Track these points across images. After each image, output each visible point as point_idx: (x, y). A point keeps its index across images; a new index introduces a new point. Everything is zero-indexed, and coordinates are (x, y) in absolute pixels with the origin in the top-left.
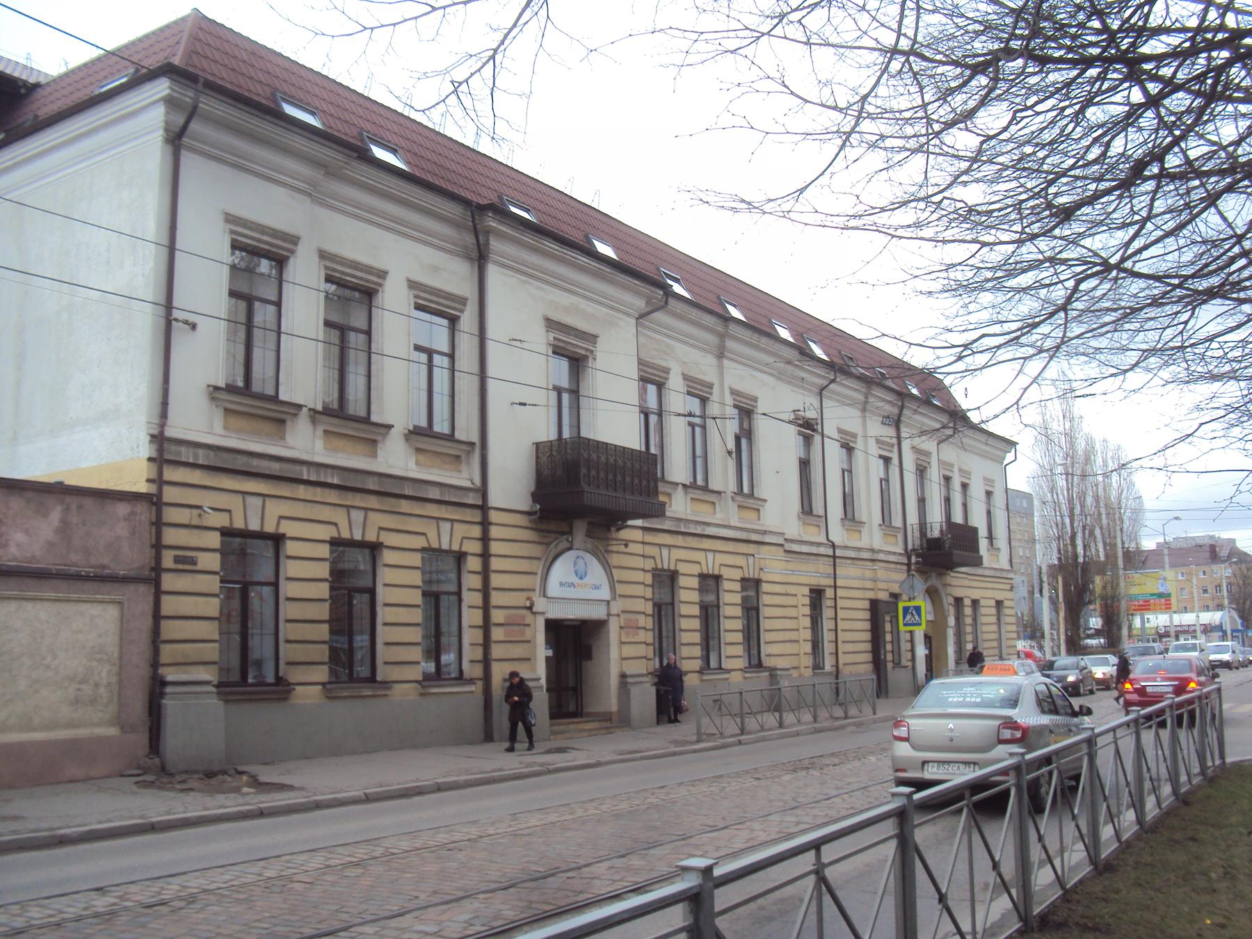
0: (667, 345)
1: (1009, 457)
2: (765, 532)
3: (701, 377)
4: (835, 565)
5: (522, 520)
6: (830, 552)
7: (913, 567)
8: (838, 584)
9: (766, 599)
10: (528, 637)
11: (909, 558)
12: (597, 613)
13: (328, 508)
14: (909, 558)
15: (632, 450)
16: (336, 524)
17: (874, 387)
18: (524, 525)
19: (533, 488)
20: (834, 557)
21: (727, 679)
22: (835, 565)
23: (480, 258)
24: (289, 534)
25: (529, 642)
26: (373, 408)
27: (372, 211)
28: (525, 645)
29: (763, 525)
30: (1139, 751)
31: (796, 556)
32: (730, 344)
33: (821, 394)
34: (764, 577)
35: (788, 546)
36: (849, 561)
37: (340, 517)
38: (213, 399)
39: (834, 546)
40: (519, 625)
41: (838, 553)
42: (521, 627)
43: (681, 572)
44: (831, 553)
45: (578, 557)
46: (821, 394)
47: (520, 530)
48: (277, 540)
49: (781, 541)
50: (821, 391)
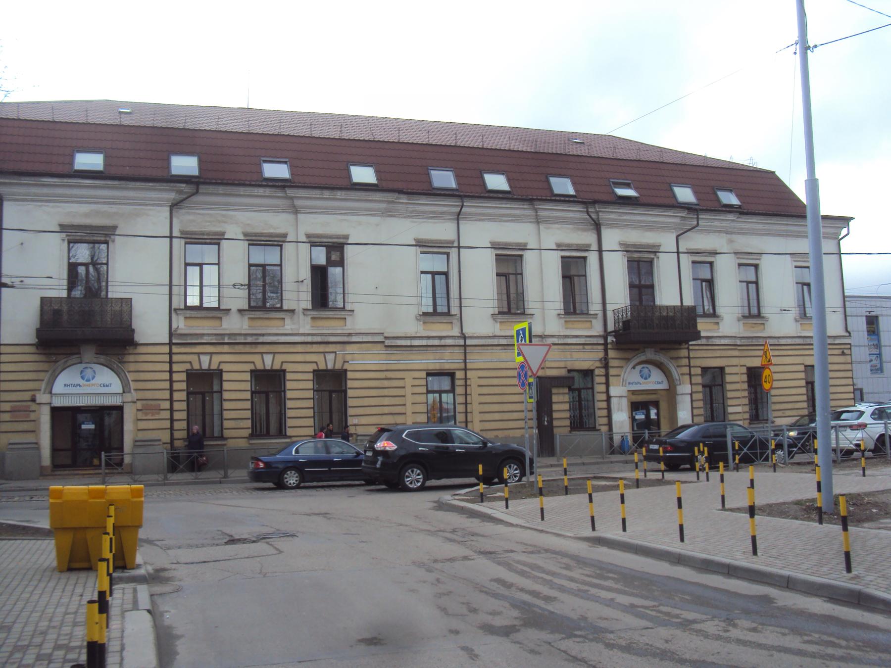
0: (223, 216)
1: (844, 232)
2: (350, 335)
3: (272, 231)
4: (465, 353)
5: (32, 349)
6: (461, 342)
7: (609, 346)
8: (468, 367)
9: (226, 386)
10: (33, 416)
11: (605, 338)
12: (116, 401)
13: (300, 355)
14: (605, 338)
15: (674, 307)
16: (253, 362)
17: (535, 203)
18: (32, 352)
19: (38, 326)
20: (465, 346)
21: (225, 445)
22: (465, 353)
23: (597, 227)
24: (348, 369)
25: (34, 421)
26: (221, 304)
27: (71, 196)
28: (33, 423)
29: (224, 329)
30: (49, 613)
31: (404, 349)
32: (298, 203)
33: (458, 220)
34: (346, 366)
35: (388, 342)
36: (500, 348)
37: (319, 358)
38: (494, 319)
39: (464, 337)
40: (27, 411)
41: (469, 342)
42: (28, 413)
43: (224, 370)
44: (463, 343)
45: (643, 368)
46: (458, 220)
47: (31, 355)
48: (220, 372)
49: (380, 338)
50: (458, 217)
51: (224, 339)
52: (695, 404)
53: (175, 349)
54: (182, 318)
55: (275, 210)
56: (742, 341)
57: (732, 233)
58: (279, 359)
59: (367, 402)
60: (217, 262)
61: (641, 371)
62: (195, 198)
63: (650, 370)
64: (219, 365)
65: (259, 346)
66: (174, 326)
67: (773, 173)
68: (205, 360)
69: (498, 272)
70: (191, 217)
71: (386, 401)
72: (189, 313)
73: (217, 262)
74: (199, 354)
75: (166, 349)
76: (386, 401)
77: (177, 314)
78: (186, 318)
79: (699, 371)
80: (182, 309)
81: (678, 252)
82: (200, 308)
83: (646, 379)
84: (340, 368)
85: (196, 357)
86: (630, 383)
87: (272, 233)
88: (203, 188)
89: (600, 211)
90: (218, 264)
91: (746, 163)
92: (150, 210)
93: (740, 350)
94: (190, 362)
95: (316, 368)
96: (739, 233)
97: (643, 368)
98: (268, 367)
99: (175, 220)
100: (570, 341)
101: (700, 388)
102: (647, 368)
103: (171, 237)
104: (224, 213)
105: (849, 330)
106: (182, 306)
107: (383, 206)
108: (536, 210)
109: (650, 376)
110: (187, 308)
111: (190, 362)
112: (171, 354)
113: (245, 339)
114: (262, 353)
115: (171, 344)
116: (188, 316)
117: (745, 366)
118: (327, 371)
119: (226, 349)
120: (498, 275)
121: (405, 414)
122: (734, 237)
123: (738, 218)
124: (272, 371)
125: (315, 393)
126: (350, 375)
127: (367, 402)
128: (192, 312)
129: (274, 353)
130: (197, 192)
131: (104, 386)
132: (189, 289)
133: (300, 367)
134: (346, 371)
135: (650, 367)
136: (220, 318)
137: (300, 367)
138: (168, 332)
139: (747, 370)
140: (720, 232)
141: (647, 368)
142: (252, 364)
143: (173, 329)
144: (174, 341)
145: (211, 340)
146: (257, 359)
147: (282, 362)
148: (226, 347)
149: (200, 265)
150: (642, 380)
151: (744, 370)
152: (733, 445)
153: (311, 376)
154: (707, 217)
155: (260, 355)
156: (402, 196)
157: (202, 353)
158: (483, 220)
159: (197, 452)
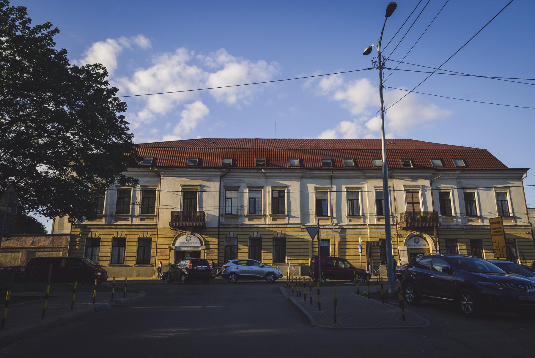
1: (525, 175)
29: (239, 222)
51: (239, 226)
52: (220, 258)
53: (221, 230)
54: (224, 218)
55: (259, 177)
56: (467, 227)
57: (460, 179)
58: (260, 233)
59: (294, 250)
60: (237, 197)
61: (414, 240)
62: (229, 174)
63: (419, 240)
64: (237, 236)
65: (252, 229)
66: (221, 221)
67: (486, 150)
68: (255, 233)
69: (377, 199)
70: (228, 181)
71: (301, 250)
72: (226, 216)
73: (237, 197)
74: (229, 231)
75: (217, 230)
76: (301, 250)
77: (222, 217)
78: (225, 218)
79: (444, 240)
80: (224, 215)
81: (523, 186)
82: (231, 214)
83: (417, 243)
84: (283, 237)
85: (228, 233)
86: (409, 245)
87: (258, 186)
88: (231, 170)
89: (393, 173)
90: (238, 198)
91: (472, 147)
92: (213, 179)
93: (465, 231)
94: (226, 235)
95: (250, 237)
96: (464, 179)
97: (415, 238)
98: (255, 237)
99: (222, 182)
100: (380, 227)
101: (445, 248)
102: (417, 238)
103: (160, 191)
104: (240, 179)
105: (530, 222)
106: (224, 214)
107: (301, 174)
108: (364, 173)
109: (419, 242)
110: (226, 214)
111: (226, 235)
112: (219, 231)
113: (247, 226)
114: (253, 231)
115: (219, 228)
116: (226, 217)
117: (469, 238)
118: (278, 238)
119: (240, 230)
120: (348, 200)
121: (309, 256)
122: (461, 180)
123: (462, 172)
124: (257, 238)
125: (250, 247)
126: (287, 240)
127: (294, 250)
128: (228, 216)
129: (258, 231)
130: (229, 172)
131: (194, 243)
132: (227, 208)
133: (268, 237)
134: (285, 238)
135: (419, 238)
136: (238, 218)
137: (268, 237)
138: (218, 223)
139: (470, 240)
140: (453, 178)
141: (417, 238)
142: (226, 235)
143: (220, 222)
144: (220, 227)
145: (234, 226)
146: (251, 233)
147: (261, 235)
148: (240, 229)
149: (231, 198)
150: (415, 244)
151: (468, 240)
152: (321, 274)
153: (272, 240)
154: (445, 172)
155: (252, 232)
156: (307, 170)
157: (235, 231)
158: (342, 178)
159: (218, 268)
